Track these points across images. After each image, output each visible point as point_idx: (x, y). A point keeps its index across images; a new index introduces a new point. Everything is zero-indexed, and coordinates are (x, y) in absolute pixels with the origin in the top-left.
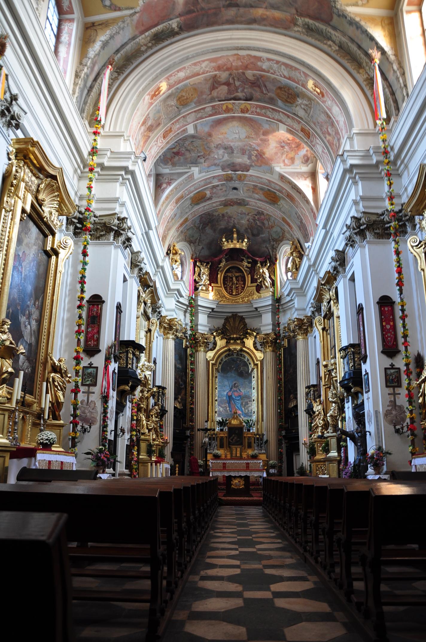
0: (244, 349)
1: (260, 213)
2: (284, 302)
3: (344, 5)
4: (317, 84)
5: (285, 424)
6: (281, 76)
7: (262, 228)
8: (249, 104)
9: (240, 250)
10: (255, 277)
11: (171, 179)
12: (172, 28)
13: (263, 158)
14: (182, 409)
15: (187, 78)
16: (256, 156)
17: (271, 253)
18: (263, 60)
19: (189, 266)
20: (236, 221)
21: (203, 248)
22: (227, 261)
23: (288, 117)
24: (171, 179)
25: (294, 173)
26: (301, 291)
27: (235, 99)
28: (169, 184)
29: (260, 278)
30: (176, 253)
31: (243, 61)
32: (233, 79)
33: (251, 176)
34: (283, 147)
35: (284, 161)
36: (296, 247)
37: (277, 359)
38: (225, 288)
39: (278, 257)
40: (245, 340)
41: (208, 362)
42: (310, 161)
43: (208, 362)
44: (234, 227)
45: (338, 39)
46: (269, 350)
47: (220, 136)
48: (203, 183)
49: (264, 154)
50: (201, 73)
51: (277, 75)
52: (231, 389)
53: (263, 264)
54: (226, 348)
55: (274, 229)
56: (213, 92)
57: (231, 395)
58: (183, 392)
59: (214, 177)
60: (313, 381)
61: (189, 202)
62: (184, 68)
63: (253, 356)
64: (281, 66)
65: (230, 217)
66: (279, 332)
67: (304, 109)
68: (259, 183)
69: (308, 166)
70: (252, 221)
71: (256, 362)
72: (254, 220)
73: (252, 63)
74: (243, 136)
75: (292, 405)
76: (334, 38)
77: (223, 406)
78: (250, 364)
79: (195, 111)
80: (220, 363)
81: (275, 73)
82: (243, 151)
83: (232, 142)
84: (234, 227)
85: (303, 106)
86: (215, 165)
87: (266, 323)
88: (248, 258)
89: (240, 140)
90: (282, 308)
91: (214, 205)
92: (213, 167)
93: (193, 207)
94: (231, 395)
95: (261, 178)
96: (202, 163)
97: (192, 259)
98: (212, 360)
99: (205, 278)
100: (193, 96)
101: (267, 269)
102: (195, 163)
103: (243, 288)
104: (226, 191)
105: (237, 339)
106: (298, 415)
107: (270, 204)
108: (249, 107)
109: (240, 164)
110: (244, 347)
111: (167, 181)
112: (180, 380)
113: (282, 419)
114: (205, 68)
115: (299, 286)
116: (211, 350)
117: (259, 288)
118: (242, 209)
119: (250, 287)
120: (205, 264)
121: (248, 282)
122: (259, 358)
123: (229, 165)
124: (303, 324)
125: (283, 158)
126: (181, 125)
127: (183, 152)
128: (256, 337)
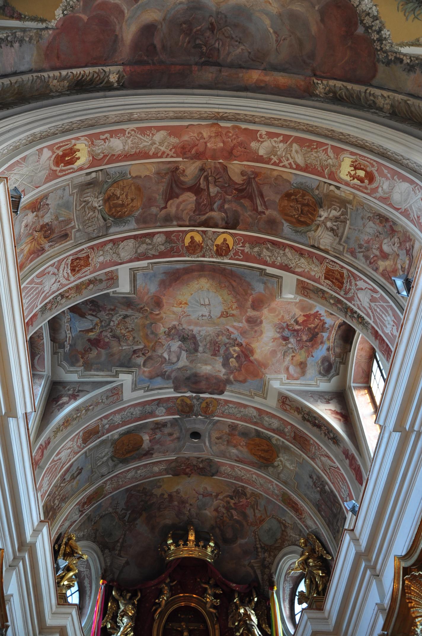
1: (239, 493)
3: (398, 45)
4: (360, 161)
6: (291, 168)
8: (231, 234)
9: (196, 565)
10: (230, 625)
11: (79, 391)
12: (108, 81)
13: (251, 362)
15: (127, 157)
16: (238, 358)
17: (260, 577)
18: (261, 136)
20: (194, 511)
21: (127, 563)
22: (173, 591)
23: (301, 253)
24: (79, 391)
25: (307, 392)
27: (206, 224)
28: (74, 397)
31: (225, 139)
32: (206, 178)
33: (227, 402)
34: (286, 339)
35: (287, 369)
36: (313, 551)
39: (275, 579)
42: (333, 372)
45: (388, 101)
47: (175, 309)
48: (137, 411)
49: (252, 352)
50: (151, 153)
51: (284, 166)
53: (245, 601)
55: (266, 526)
56: (170, 203)
59: (159, 402)
61: (107, 450)
62: (123, 131)
64: (291, 145)
65: (183, 502)
67: (332, 230)
68: (240, 420)
69: (329, 380)
70: (223, 510)
72: (228, 509)
73: (241, 144)
74: (216, 312)
76: (380, 102)
79: (135, 237)
81: (280, 161)
82: (215, 348)
83: (196, 324)
85: (329, 224)
86: (164, 375)
88: (216, 586)
89: (211, 321)
91: (156, 469)
92: (159, 379)
93: (115, 466)
95: (245, 406)
96: (139, 366)
97: (103, 578)
100: (134, 204)
102: (126, 364)
104: (178, 438)
107: (259, 468)
108: (230, 241)
109: (208, 378)
111: (70, 392)
114: (161, 144)
118: (206, 485)
123: (188, 379)
125: (286, 363)
126: (108, 258)
127: (107, 340)
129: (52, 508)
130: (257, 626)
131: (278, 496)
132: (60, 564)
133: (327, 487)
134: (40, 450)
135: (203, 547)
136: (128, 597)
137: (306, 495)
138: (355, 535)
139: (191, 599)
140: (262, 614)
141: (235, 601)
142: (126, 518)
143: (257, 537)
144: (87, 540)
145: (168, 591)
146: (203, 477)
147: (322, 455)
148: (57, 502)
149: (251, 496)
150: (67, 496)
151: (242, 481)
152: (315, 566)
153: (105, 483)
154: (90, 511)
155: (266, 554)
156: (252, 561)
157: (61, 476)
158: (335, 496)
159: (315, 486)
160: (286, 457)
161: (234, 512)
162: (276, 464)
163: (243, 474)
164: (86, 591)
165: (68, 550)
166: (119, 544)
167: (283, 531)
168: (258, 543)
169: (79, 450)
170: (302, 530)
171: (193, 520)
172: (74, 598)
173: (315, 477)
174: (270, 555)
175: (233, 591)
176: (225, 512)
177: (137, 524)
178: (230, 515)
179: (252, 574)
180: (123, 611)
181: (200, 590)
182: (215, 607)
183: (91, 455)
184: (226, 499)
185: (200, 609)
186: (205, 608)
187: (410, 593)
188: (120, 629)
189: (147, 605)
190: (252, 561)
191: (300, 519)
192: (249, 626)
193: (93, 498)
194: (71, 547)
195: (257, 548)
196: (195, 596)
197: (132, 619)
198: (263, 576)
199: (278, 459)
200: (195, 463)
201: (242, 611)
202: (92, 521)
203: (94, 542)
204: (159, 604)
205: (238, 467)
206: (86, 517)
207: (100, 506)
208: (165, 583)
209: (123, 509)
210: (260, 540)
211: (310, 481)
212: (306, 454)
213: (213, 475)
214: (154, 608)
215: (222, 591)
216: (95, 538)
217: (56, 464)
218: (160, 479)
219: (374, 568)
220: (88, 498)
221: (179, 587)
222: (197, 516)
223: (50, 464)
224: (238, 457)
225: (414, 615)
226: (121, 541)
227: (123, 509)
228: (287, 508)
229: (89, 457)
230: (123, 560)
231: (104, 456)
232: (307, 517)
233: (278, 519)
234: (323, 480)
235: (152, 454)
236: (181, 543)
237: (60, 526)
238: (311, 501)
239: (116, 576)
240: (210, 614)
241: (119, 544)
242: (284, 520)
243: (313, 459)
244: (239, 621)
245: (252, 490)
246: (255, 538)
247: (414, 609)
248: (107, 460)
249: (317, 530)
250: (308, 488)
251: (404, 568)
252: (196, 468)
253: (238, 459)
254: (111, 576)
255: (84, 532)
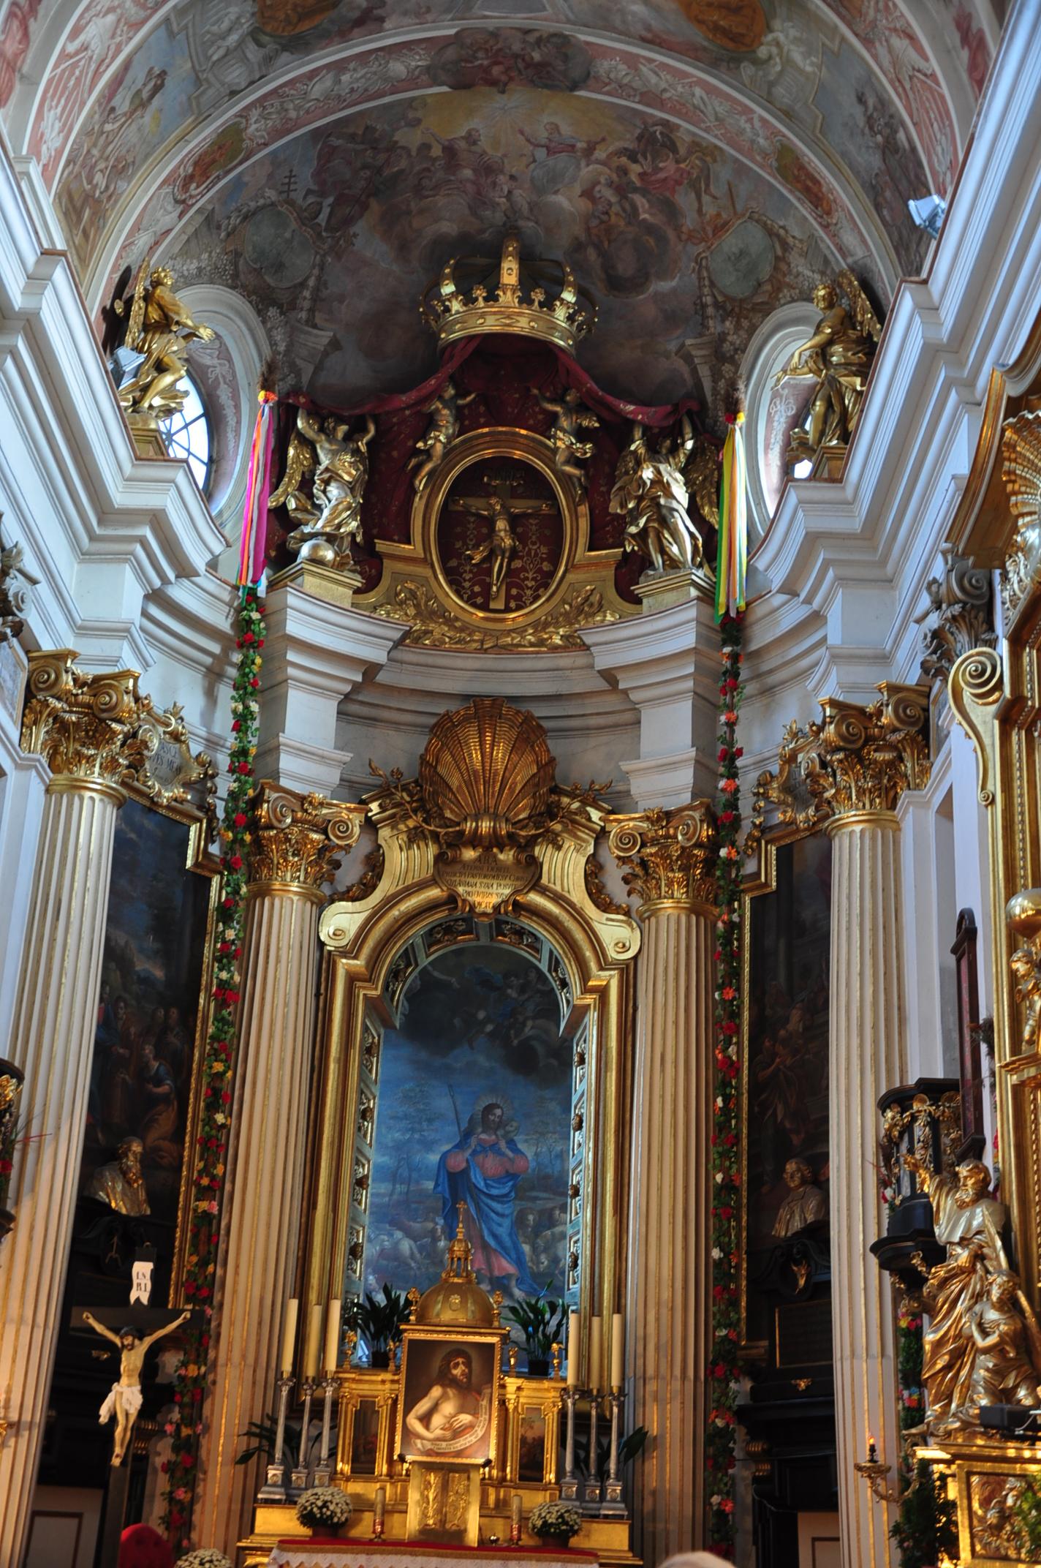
0: (535, 898)
1: (655, 142)
2: (769, 638)
5: (753, 1335)
7: (662, 239)
9: (531, 353)
10: (615, 508)
14: (141, 1220)
17: (707, 384)
19: (253, 424)
20: (522, 197)
21: (335, 344)
22: (465, 420)
26: (864, 553)
29: (634, 516)
30: (164, 324)
36: (849, 320)
37: (720, 951)
38: (448, 573)
40: (543, 852)
41: (324, 961)
43: (324, 961)
44: (510, 230)
46: (671, 905)
52: (467, 1135)
54: (434, 893)
55: (730, 242)
57: (465, 1172)
58: (165, 1121)
60: (928, 1058)
63: (579, 935)
65: (488, 170)
66: (733, 804)
71: (600, 977)
72: (623, 190)
75: (797, 1225)
77: (416, 1226)
78: (564, 984)
80: (395, 974)
84: (510, 230)
87: (661, 762)
88: (581, 408)
90: (758, 676)
91: (398, 68)
93: (269, 60)
94: (465, 1172)
97: (267, 385)
98: (351, 951)
99: (336, 504)
101: (683, 471)
103: (545, 580)
105: (497, 842)
106: (827, 1285)
107: (714, 64)
110: (536, 884)
112: (149, 1050)
113: (734, 1303)
115: (856, 524)
116: (348, 896)
117: (630, 576)
118: (554, 116)
119: (587, 567)
120: (343, 429)
121: (574, 543)
122: (612, 954)
124: (869, 739)
128: (601, 835)
129: (88, 198)
130: (689, 512)
131: (765, 155)
132: (123, 362)
133: (901, 135)
134: (16, 24)
135: (541, 305)
136: (340, 435)
137: (844, 155)
138: (929, 294)
139: (514, 441)
140: (704, 480)
141: (633, 448)
142: (322, 219)
143: (705, 274)
144: (212, 282)
145: (451, 419)
146: (546, 91)
147: (895, 30)
148: (99, 179)
149: (690, 153)
150: (130, 160)
151: (661, 105)
152: (847, 364)
153: (244, 114)
154: (209, 201)
155: (728, 323)
156: (688, 342)
157: (98, 101)
158: (920, 164)
159: (871, 128)
160: (793, 33)
161: (640, 200)
162: (762, 52)
163: (663, 85)
164: (225, 416)
165: (154, 315)
166: (307, 294)
167: (777, 258)
168: (706, 291)
169: (143, 14)
170: (830, 257)
171: (521, 223)
172: (191, 438)
173: (871, 101)
174: (738, 327)
175: (629, 424)
176: (613, 199)
177: (355, 235)
178: (627, 207)
179: (687, 376)
180: (327, 470)
181: (540, 417)
182: (578, 463)
183: (186, 27)
184: (616, 162)
185: (539, 464)
186: (551, 463)
187: (1015, 461)
188: (321, 511)
189: (395, 454)
190: (688, 342)
191: (826, 227)
192: (664, 511)
193: (214, 161)
194: (161, 307)
195: (704, 306)
196: (523, 432)
197: (352, 490)
198: (715, 381)
199: (770, 37)
200: (516, 47)
201: (648, 474)
202: (219, 227)
203: (233, 288)
204: (428, 453)
205: (651, 61)
206: (201, 219)
207: (238, 184)
208: (441, 398)
209: (309, 192)
210: (712, 284)
211: (858, 111)
212: (849, 25)
213: (575, 86)
214: (413, 462)
215: (598, 421)
216: (235, 276)
217: (75, 65)
218: (413, 99)
219: (971, 383)
220: (196, 164)
221: (482, 409)
222: (531, 210)
223: (56, 66)
224: (648, 28)
225: (1014, 511)
226: (311, 282)
227: (309, 192)
228: (791, 191)
229: (181, 37)
230: (322, 338)
231: (230, 30)
232: (845, 222)
233: (765, 224)
234: (892, 110)
235: (382, 20)
236: (480, 293)
237: (124, 248)
238: (857, 174)
239: (305, 379)
240: (565, 479)
241: (307, 294)
242: (783, 227)
243: (868, 42)
244: (640, 499)
245: (694, 134)
246: (700, 279)
247: (1020, 497)
248: (241, 44)
249: (868, 261)
250: (852, 134)
251: (1009, 398)
252: (521, 65)
253: (649, 36)
254: (291, 380)
255: (199, 260)
